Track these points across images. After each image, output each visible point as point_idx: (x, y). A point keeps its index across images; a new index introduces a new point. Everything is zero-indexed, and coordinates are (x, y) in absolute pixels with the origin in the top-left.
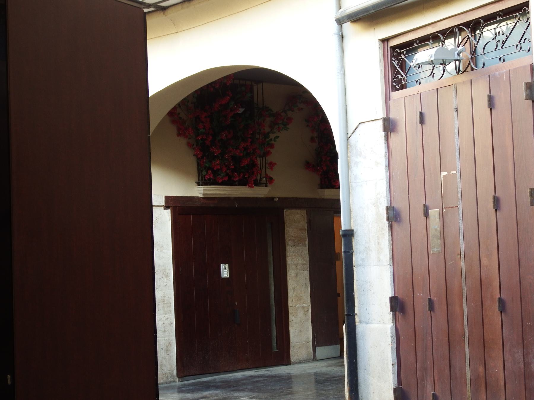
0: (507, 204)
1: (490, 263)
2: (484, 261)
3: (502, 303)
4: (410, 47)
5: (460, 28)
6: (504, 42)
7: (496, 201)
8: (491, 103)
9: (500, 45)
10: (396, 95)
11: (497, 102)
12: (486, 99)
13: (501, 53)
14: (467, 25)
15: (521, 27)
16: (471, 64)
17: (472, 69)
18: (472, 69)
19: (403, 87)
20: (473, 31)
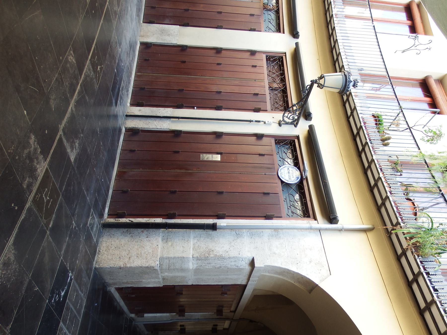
0: (218, 97)
1: (201, 7)
2: (202, 5)
3: (188, 10)
4: (294, 151)
5: (278, 6)
6: (270, 22)
7: (220, 13)
8: (252, 15)
9: (269, 20)
10: (273, 141)
11: (252, 17)
12: (254, 14)
13: (267, 21)
14: (278, 9)
15: (273, 29)
16: (265, 8)
17: (264, 9)
18: (264, 9)
19: (276, 143)
20: (276, 11)
